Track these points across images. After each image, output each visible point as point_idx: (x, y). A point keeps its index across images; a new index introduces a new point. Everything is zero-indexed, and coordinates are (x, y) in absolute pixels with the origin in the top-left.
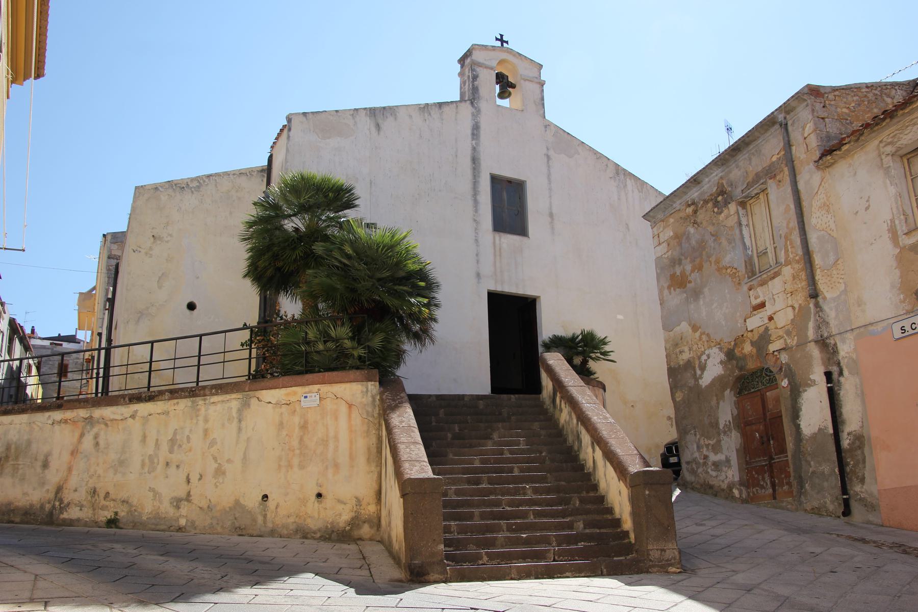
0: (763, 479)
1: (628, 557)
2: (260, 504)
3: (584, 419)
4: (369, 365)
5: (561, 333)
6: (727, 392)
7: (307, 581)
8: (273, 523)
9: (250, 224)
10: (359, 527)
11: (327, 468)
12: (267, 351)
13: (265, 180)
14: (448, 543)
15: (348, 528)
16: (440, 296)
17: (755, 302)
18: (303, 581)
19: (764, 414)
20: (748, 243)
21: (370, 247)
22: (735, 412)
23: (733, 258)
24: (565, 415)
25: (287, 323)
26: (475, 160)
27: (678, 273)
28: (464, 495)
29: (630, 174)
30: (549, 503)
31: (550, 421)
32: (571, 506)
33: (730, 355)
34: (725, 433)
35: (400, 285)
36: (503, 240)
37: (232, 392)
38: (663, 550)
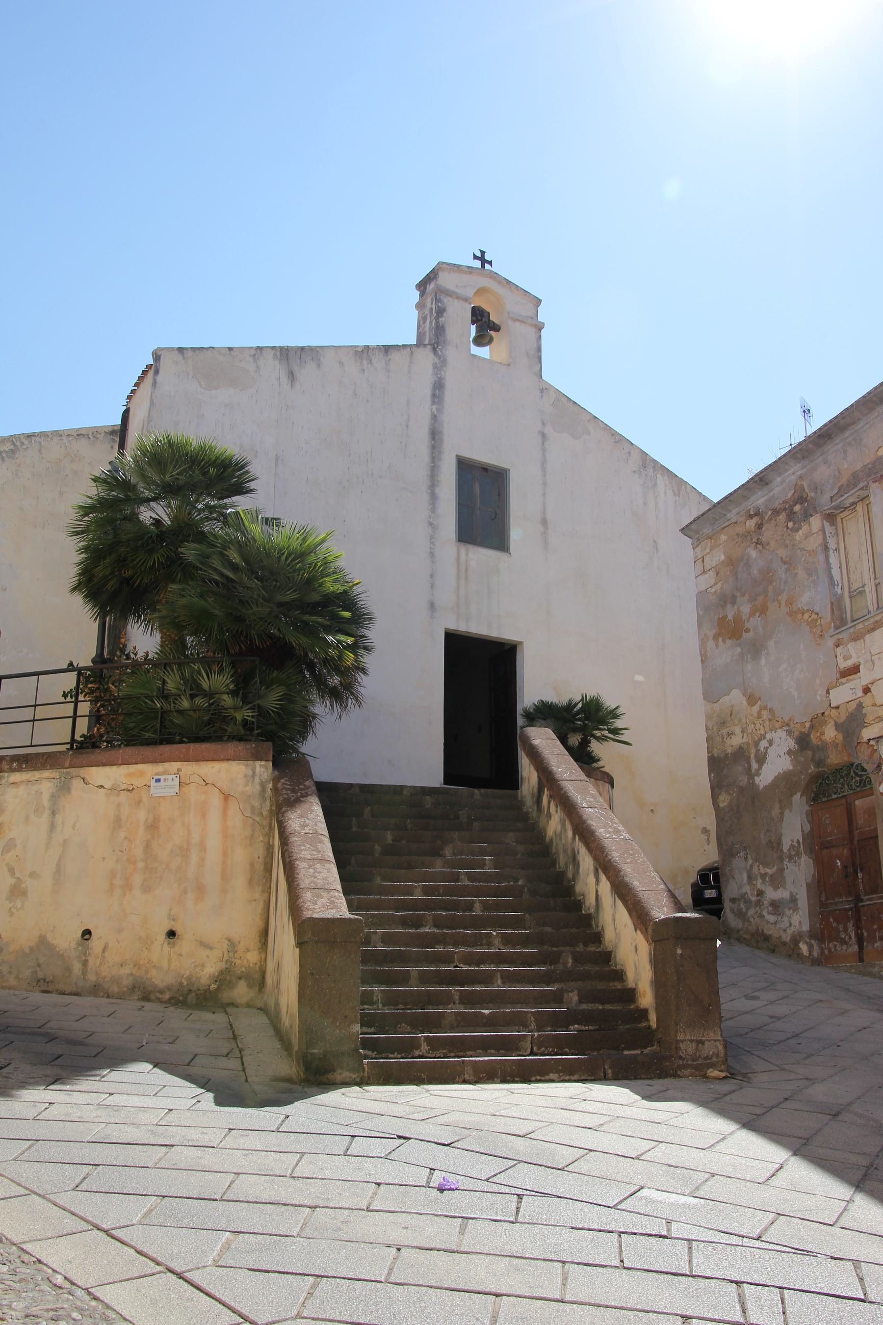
0: (845, 930)
1: (646, 1051)
2: (79, 944)
3: (584, 832)
4: (258, 735)
5: (551, 697)
6: (797, 797)
7: (139, 1078)
8: (97, 974)
9: (86, 510)
10: (231, 985)
11: (185, 892)
12: (102, 706)
13: (116, 447)
14: (367, 1021)
15: (213, 987)
16: (373, 634)
17: (844, 665)
18: (133, 1077)
19: (851, 832)
20: (835, 573)
21: (268, 555)
22: (807, 828)
23: (813, 597)
24: (555, 824)
25: (136, 665)
26: (435, 435)
27: (730, 617)
28: (396, 944)
29: (663, 467)
30: (526, 960)
31: (534, 834)
32: (560, 967)
33: (803, 741)
34: (790, 858)
35: (311, 614)
36: (471, 555)
37: (43, 767)
38: (700, 1042)
